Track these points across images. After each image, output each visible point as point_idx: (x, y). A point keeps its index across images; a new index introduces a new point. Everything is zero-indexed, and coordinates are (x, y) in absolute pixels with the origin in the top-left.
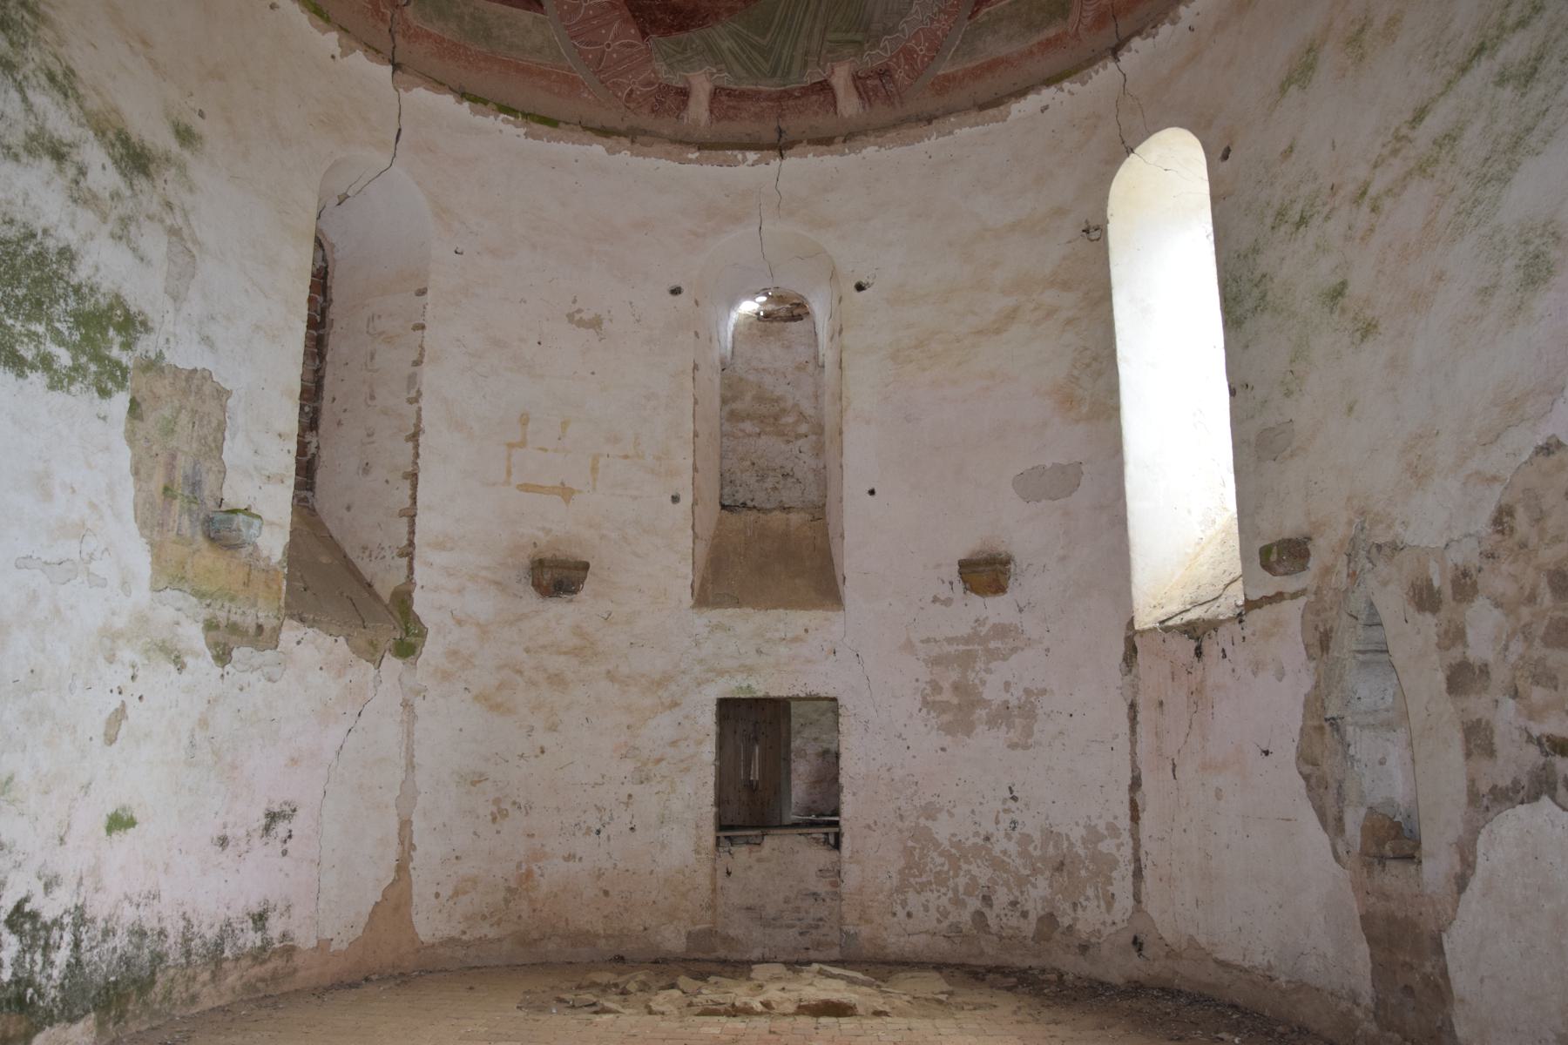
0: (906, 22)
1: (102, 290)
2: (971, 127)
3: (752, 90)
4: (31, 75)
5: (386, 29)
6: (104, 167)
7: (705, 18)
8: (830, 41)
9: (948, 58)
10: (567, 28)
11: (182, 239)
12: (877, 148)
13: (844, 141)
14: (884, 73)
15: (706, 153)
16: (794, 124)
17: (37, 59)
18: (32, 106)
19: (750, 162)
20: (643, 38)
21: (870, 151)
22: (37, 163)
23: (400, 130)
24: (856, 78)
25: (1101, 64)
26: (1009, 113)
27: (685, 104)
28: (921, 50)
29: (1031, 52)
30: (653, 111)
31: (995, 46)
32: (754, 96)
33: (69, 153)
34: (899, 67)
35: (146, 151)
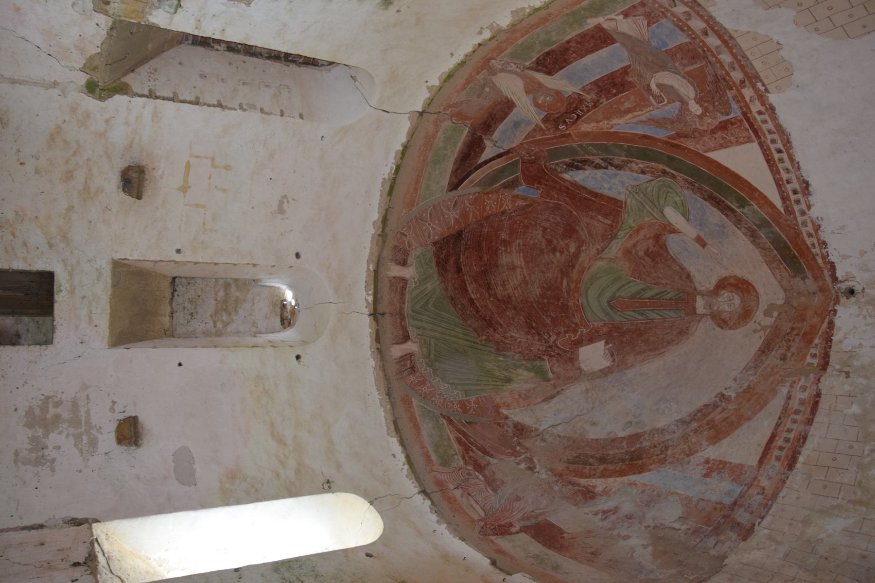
2: (385, 416)
3: (405, 299)
7: (443, 275)
9: (421, 404)
10: (439, 203)
12: (374, 366)
13: (378, 349)
14: (413, 369)
15: (373, 274)
16: (387, 321)
19: (368, 298)
21: (372, 363)
23: (388, 112)
26: (392, 437)
27: (399, 264)
30: (395, 247)
31: (427, 428)
32: (402, 301)
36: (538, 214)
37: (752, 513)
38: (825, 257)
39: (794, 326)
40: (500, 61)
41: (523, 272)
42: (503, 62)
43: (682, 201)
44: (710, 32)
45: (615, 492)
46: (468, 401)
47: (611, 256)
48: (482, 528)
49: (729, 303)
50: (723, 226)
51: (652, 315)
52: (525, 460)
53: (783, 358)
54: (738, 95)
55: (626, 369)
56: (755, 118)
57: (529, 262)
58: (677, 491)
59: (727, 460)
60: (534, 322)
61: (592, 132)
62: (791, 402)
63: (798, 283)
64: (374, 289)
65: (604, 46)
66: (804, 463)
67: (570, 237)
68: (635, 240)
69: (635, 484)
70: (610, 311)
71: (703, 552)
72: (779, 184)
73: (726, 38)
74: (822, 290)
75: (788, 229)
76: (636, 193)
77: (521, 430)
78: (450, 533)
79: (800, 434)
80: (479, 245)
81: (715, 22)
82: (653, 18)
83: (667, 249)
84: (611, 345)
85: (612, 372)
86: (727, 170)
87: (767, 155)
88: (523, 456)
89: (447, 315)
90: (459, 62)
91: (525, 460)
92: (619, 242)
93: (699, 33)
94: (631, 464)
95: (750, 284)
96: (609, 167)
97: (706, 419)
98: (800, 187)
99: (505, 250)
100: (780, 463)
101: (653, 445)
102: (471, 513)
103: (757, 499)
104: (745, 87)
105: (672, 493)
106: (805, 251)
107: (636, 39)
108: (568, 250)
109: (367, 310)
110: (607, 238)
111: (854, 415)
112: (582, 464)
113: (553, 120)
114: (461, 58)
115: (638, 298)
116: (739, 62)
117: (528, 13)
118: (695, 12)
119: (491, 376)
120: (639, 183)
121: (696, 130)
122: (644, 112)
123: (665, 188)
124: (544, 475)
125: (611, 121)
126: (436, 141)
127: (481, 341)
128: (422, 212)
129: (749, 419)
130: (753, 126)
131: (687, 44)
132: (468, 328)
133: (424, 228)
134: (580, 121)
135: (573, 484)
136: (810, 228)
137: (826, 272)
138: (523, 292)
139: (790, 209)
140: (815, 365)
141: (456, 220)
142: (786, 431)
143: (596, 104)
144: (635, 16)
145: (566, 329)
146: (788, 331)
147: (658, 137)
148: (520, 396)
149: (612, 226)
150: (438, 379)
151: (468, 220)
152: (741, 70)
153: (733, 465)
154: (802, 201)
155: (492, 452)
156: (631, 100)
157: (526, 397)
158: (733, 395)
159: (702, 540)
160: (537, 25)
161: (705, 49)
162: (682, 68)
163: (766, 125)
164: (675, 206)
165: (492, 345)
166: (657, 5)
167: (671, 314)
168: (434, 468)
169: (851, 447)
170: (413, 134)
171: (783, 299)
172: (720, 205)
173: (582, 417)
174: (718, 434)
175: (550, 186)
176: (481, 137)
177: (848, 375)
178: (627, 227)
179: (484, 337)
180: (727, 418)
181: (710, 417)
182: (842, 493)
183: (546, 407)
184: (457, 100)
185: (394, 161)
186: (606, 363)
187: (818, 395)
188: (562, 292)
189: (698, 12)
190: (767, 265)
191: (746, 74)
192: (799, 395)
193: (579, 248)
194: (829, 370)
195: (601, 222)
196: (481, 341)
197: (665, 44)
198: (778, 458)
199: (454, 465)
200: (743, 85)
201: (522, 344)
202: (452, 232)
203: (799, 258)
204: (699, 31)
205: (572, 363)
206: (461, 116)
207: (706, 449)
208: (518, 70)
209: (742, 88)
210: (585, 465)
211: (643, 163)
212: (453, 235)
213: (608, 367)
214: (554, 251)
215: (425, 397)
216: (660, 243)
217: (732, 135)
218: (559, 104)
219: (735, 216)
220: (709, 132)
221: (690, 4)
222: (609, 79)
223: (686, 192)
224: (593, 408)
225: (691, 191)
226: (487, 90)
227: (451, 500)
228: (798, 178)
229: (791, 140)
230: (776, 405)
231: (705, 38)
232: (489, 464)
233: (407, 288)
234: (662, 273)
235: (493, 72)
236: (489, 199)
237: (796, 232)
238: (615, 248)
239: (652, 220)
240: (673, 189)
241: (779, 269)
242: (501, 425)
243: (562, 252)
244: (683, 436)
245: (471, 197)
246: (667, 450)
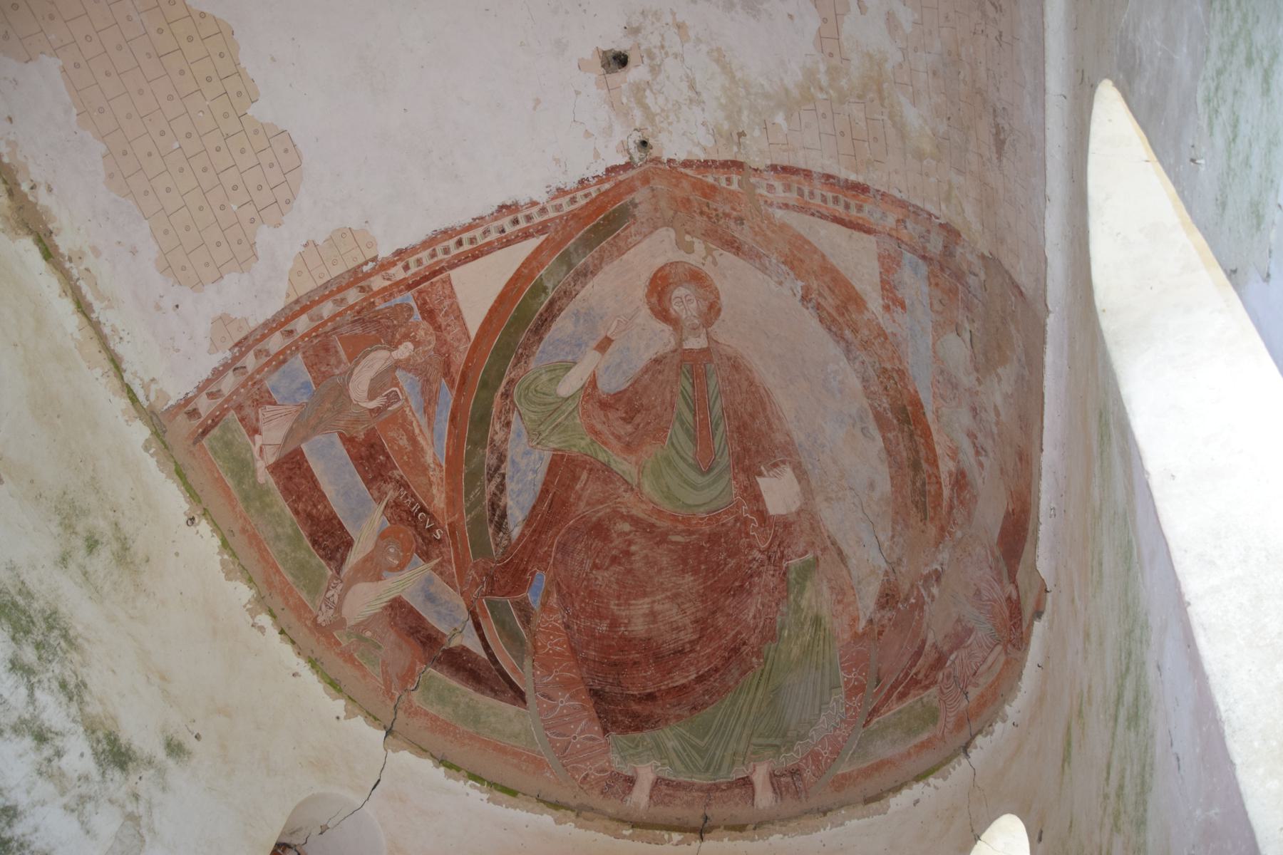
0: (815, 730)
1: (32, 848)
2: (858, 819)
3: (687, 782)
4: (46, 680)
5: (393, 705)
6: (82, 755)
7: (657, 722)
8: (755, 745)
9: (847, 760)
10: (543, 721)
11: (139, 825)
12: (781, 836)
13: (755, 829)
14: (795, 773)
15: (638, 831)
16: (718, 811)
17: (57, 671)
18: (35, 700)
19: (675, 842)
20: (604, 734)
21: (776, 838)
22: (18, 740)
23: (379, 781)
24: (773, 776)
25: (955, 760)
26: (889, 807)
27: (630, 789)
28: (826, 753)
29: (909, 754)
30: (602, 793)
31: (883, 749)
32: (688, 787)
33: (52, 738)
34: (808, 767)
35: (130, 752)
36: (572, 576)
37: (928, 231)
38: (600, 180)
39: (698, 211)
40: (320, 609)
41: (659, 601)
42: (323, 607)
43: (547, 372)
44: (288, 328)
45: (951, 440)
46: (846, 683)
47: (634, 471)
48: (1014, 646)
49: (684, 301)
50: (577, 314)
51: (717, 409)
52: (927, 588)
53: (740, 221)
55: (793, 444)
56: (415, 274)
57: (645, 591)
58: (930, 347)
59: (879, 279)
60: (733, 583)
61: (447, 492)
62: (791, 203)
63: (642, 211)
64: (661, 829)
65: (306, 464)
66: (857, 172)
67: (608, 530)
68: (610, 436)
69: (937, 412)
70: (716, 471)
71: (986, 290)
73: (298, 308)
74: (646, 180)
75: (568, 229)
76: (540, 434)
77: (888, 598)
78: (1016, 697)
79: (825, 184)
80: (616, 665)
81: (274, 320)
83: (620, 392)
84: (762, 468)
85: (800, 463)
86: (493, 311)
87: (466, 258)
88: (923, 591)
89: (718, 717)
90: (308, 666)
91: (927, 588)
92: (614, 460)
93: (288, 341)
94: (914, 421)
95: (655, 275)
96: (502, 471)
97: (838, 318)
99: (625, 627)
100: (864, 205)
101: (885, 392)
102: (998, 667)
103: (912, 229)
104: (369, 286)
105: (934, 352)
106: (596, 206)
107: (296, 421)
108: (627, 534)
109: (693, 842)
110: (609, 477)
111: (788, 119)
112: (925, 497)
113: (427, 546)
114: (302, 661)
115: (695, 431)
116: (332, 294)
117: (230, 556)
118: (256, 344)
119: (810, 648)
120: (524, 431)
121: (437, 351)
122: (413, 419)
123: (530, 394)
124: (944, 556)
125: (429, 465)
126: (441, 717)
127: (759, 665)
128: (553, 747)
129: (823, 256)
130: (426, 276)
131: (305, 357)
132: (740, 685)
133: (578, 746)
134: (431, 510)
135: (951, 507)
136: (564, 201)
137: (621, 178)
138: (690, 601)
139: (540, 227)
140: (740, 177)
141: (572, 697)
142: (826, 203)
143: (402, 484)
144: (257, 420)
145: (743, 535)
146: (705, 218)
147: (452, 401)
148: (839, 602)
149: (591, 470)
150: (812, 733)
151: (573, 678)
152: (344, 290)
153: (882, 270)
154: (528, 213)
155: (919, 641)
156: (395, 435)
157: (842, 594)
158: (800, 283)
159: (974, 295)
160: (263, 553)
161: (314, 334)
162: (343, 365)
164: (555, 380)
165: (766, 647)
166: (242, 390)
167: (712, 383)
168: (939, 734)
169: (824, 116)
170: (420, 747)
171: (667, 230)
172: (546, 319)
173: (864, 505)
174: (851, 299)
175: (530, 557)
176: (444, 651)
177: (741, 135)
178: (592, 448)
179: (754, 660)
180: (828, 287)
181: (834, 314)
182: (876, 116)
183: (854, 561)
184: (379, 679)
185: (462, 782)
186: (788, 472)
187: (774, 168)
188: (689, 542)
189: (257, 340)
190: (623, 254)
192: (780, 194)
193: (624, 518)
194: (741, 159)
195: (585, 484)
196: (759, 665)
197: (305, 385)
198: (860, 208)
199: (936, 703)
200: (367, 289)
201: (766, 601)
202: (590, 705)
203: (607, 212)
204: (286, 340)
205: (791, 524)
206: (407, 677)
207: (873, 313)
208: (340, 587)
210: (925, 491)
211: (493, 425)
212: (595, 703)
213: (794, 470)
214: (628, 554)
215: (837, 752)
216: (612, 402)
217: (441, 302)
218: (401, 535)
219: (559, 298)
221: (243, 349)
222: (361, 463)
223: (532, 365)
224: (851, 489)
225: (531, 358)
226: (368, 634)
227: (982, 703)
228: (496, 219)
230: (799, 223)
232: (934, 646)
233: (669, 778)
234: (656, 399)
235: (340, 623)
236: (544, 647)
237: (572, 219)
238: (623, 465)
239: (578, 413)
240: (530, 384)
241: (627, 238)
242: (881, 629)
243: (630, 543)
244: (865, 349)
245: (538, 673)
246: (887, 370)
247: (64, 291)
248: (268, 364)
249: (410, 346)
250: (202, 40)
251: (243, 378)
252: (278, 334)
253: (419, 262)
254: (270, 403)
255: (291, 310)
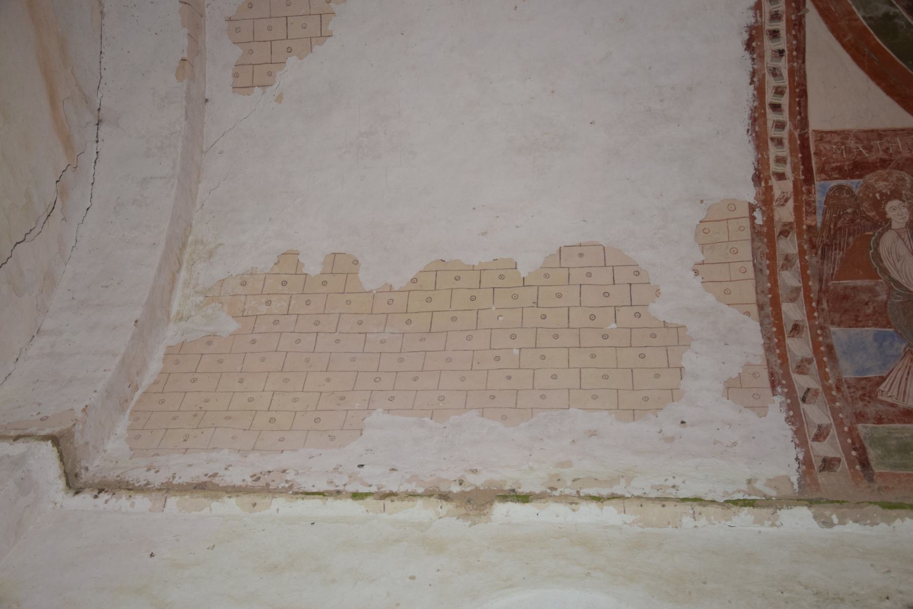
44: (788, 328)
54: (804, 215)
56: (794, 169)
72: (799, 51)
82: (863, 388)
86: (890, 91)
93: (807, 334)
98: (762, 41)
104: (785, 225)
139: (793, 4)
144: (892, 405)
152: (775, 253)
154: (767, 16)
161: (814, 304)
162: (877, 288)
163: (780, 154)
166: (838, 404)
189: (782, 364)
191: (772, 245)
200: (787, 228)
209: (791, 223)
217: (849, 151)
220: (893, 164)
228: (761, 57)
229: (750, 122)
231: (803, 321)
247: (571, 504)
248: (821, 365)
249: (895, 203)
250: (435, 290)
251: (821, 397)
252: (789, 342)
253: (780, 160)
254: (879, 384)
255: (768, 317)
